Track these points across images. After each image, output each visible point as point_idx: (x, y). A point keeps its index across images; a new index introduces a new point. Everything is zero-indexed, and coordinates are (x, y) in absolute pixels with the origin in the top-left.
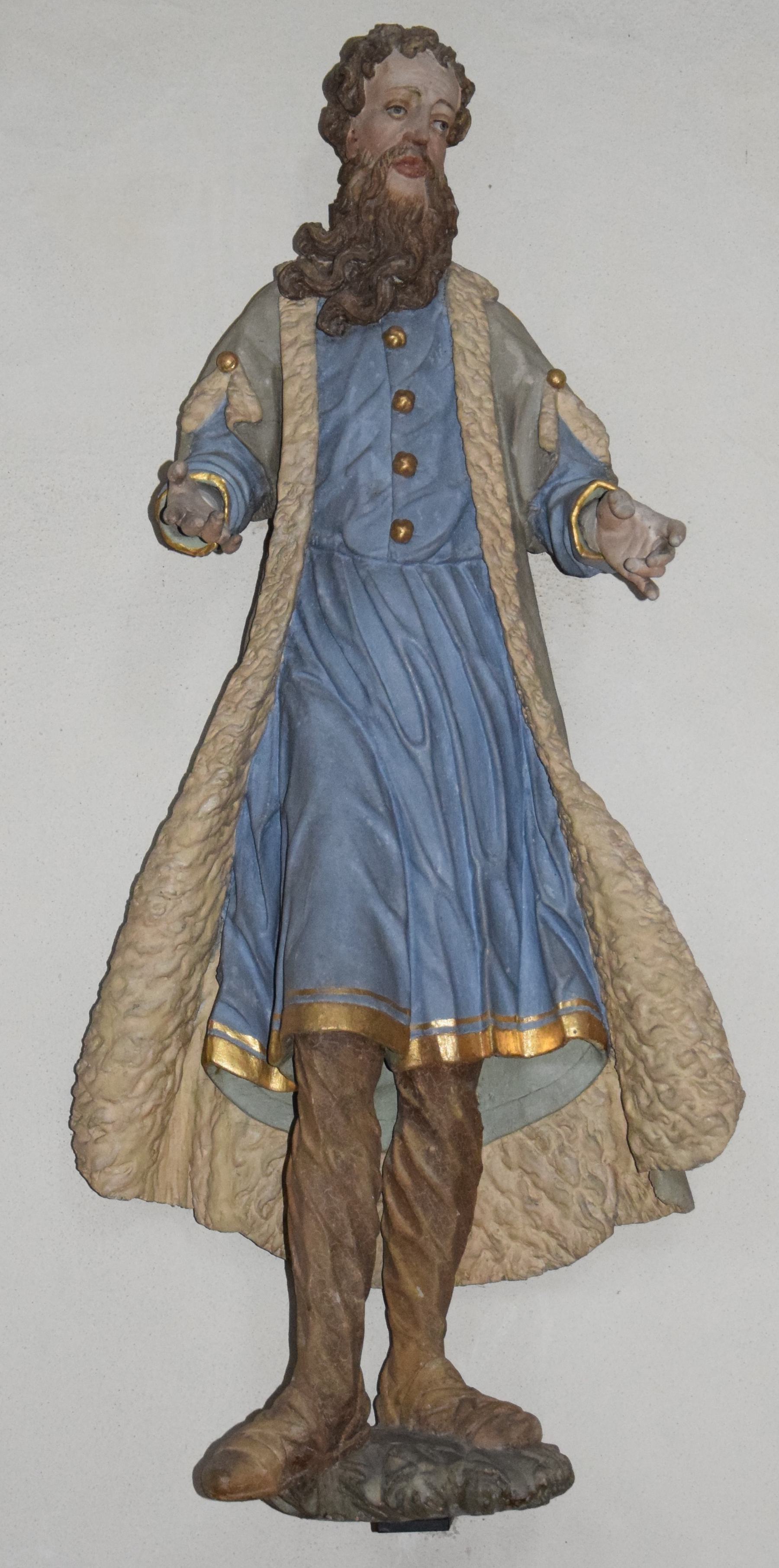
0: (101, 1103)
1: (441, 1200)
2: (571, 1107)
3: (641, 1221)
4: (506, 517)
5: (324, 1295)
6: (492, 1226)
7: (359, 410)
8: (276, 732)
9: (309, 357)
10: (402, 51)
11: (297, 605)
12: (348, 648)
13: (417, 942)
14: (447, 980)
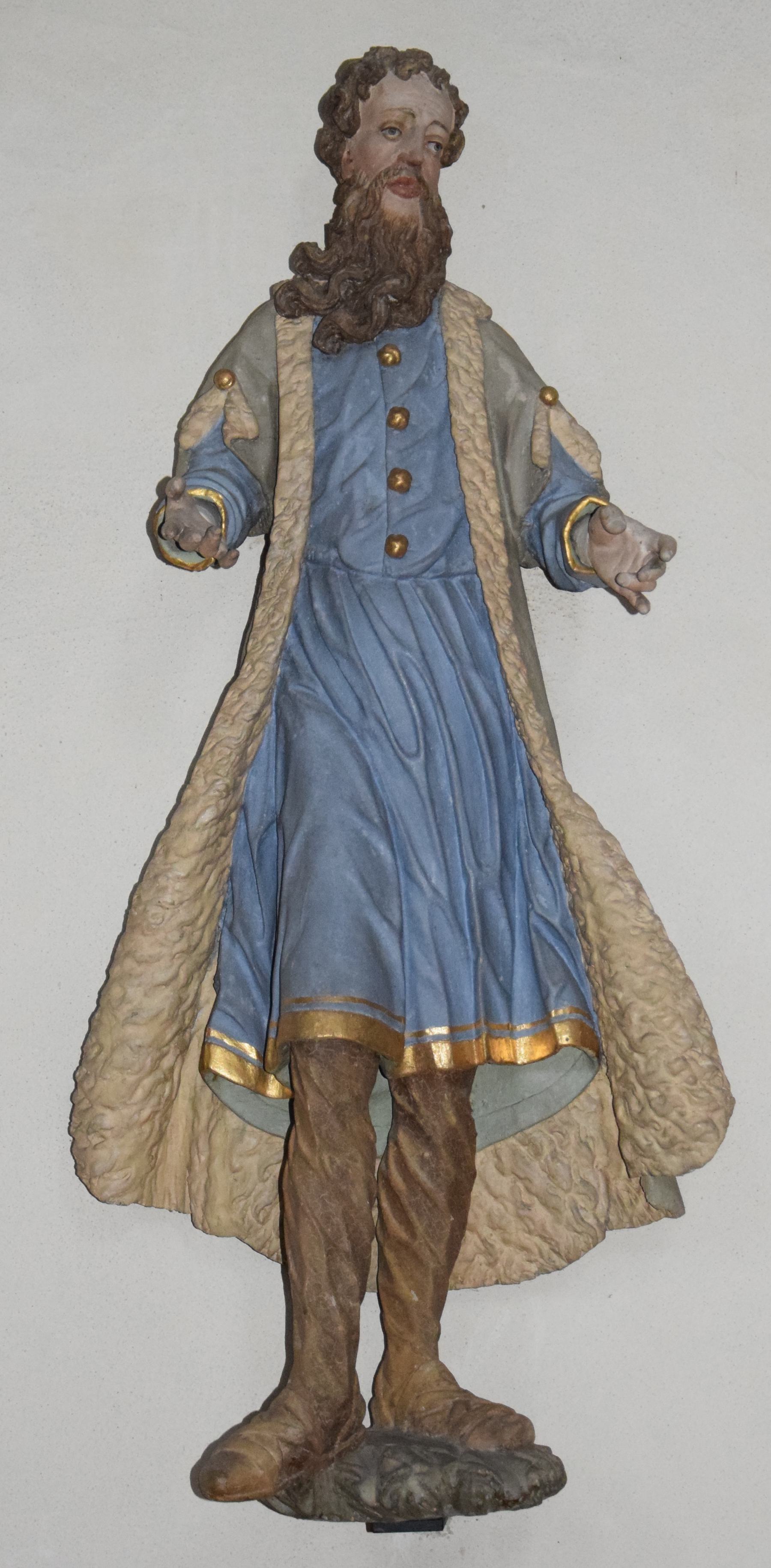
0: (100, 1110)
1: (436, 1205)
2: (563, 1114)
3: (633, 1226)
4: (500, 532)
5: (320, 1299)
6: (486, 1231)
7: (354, 427)
8: (273, 744)
9: (305, 375)
10: (396, 73)
11: (293, 619)
12: (343, 662)
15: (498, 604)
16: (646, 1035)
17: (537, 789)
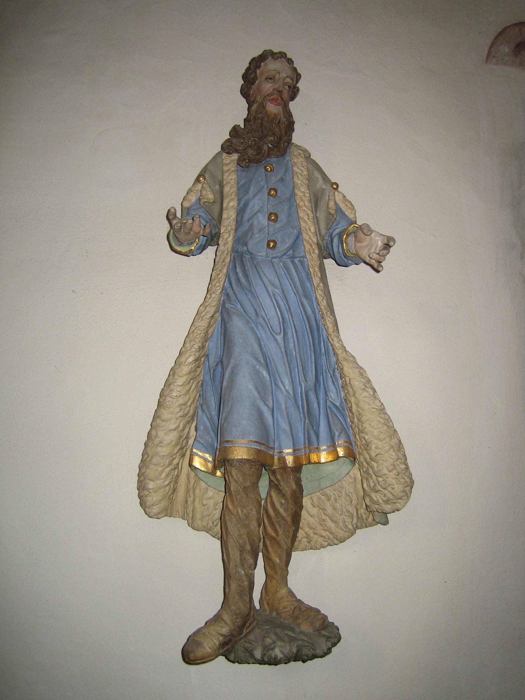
0: (148, 481)
1: (287, 523)
2: (340, 483)
3: (366, 527)
4: (315, 240)
5: (237, 571)
6: (307, 529)
7: (254, 196)
8: (220, 329)
9: (234, 176)
10: (272, 58)
11: (228, 276)
12: (248, 293)
13: (277, 418)
14: (290, 434)
15: (314, 270)
16: (377, 455)
17: (331, 348)
